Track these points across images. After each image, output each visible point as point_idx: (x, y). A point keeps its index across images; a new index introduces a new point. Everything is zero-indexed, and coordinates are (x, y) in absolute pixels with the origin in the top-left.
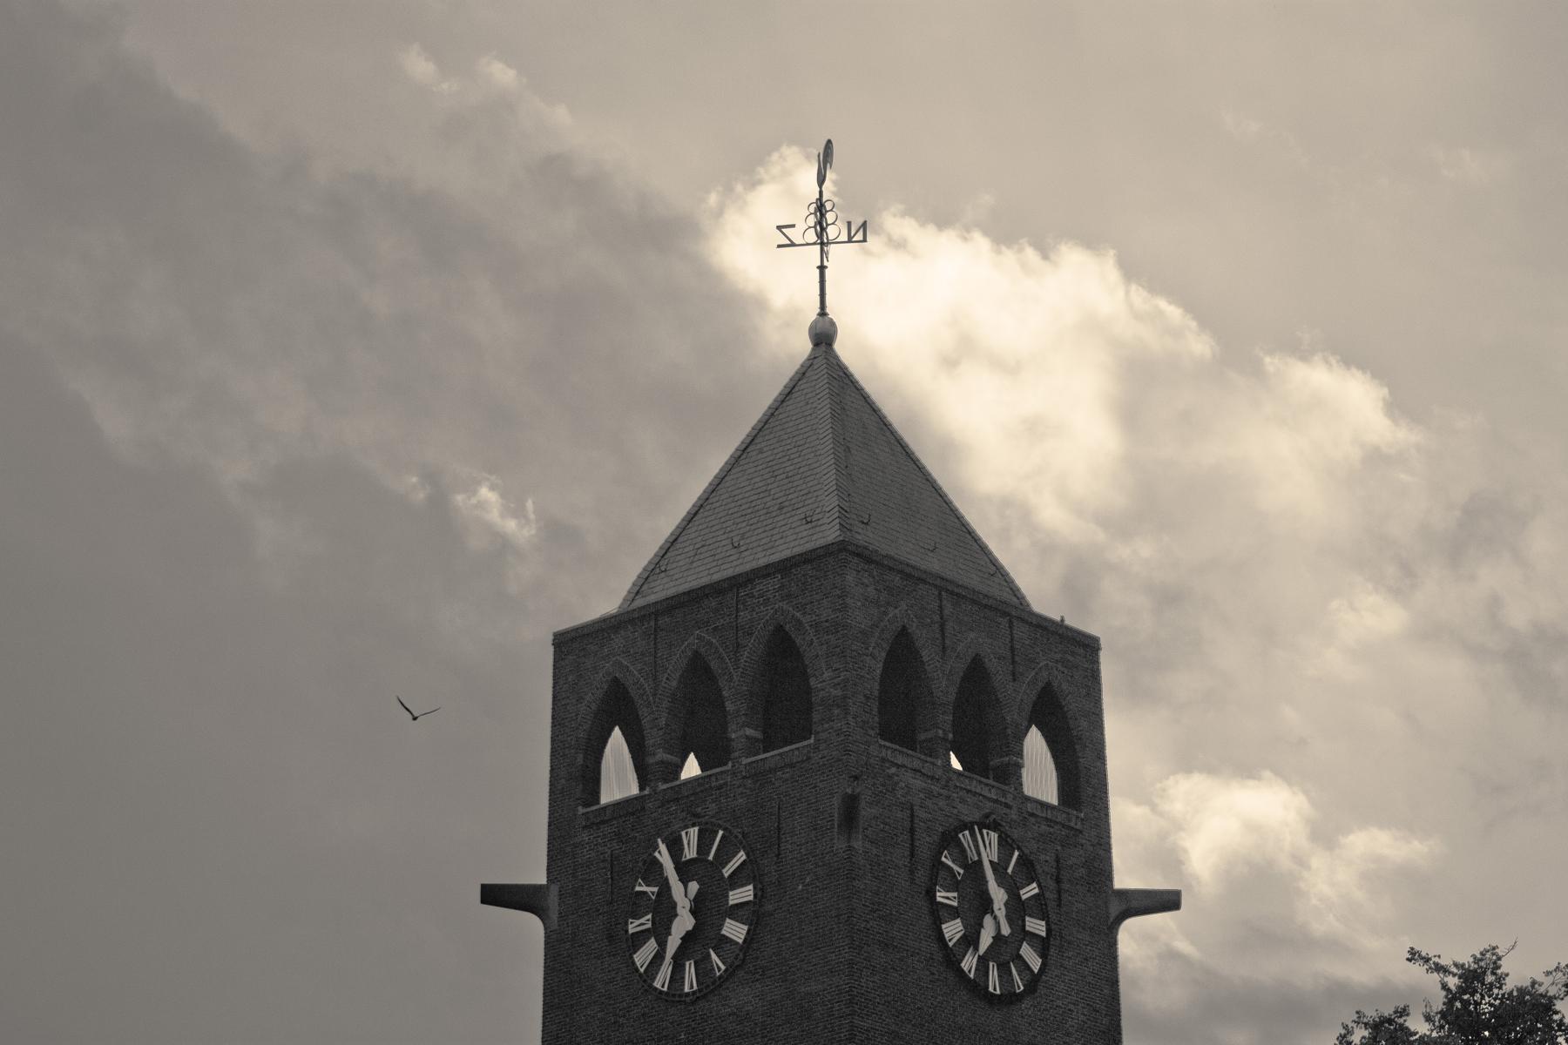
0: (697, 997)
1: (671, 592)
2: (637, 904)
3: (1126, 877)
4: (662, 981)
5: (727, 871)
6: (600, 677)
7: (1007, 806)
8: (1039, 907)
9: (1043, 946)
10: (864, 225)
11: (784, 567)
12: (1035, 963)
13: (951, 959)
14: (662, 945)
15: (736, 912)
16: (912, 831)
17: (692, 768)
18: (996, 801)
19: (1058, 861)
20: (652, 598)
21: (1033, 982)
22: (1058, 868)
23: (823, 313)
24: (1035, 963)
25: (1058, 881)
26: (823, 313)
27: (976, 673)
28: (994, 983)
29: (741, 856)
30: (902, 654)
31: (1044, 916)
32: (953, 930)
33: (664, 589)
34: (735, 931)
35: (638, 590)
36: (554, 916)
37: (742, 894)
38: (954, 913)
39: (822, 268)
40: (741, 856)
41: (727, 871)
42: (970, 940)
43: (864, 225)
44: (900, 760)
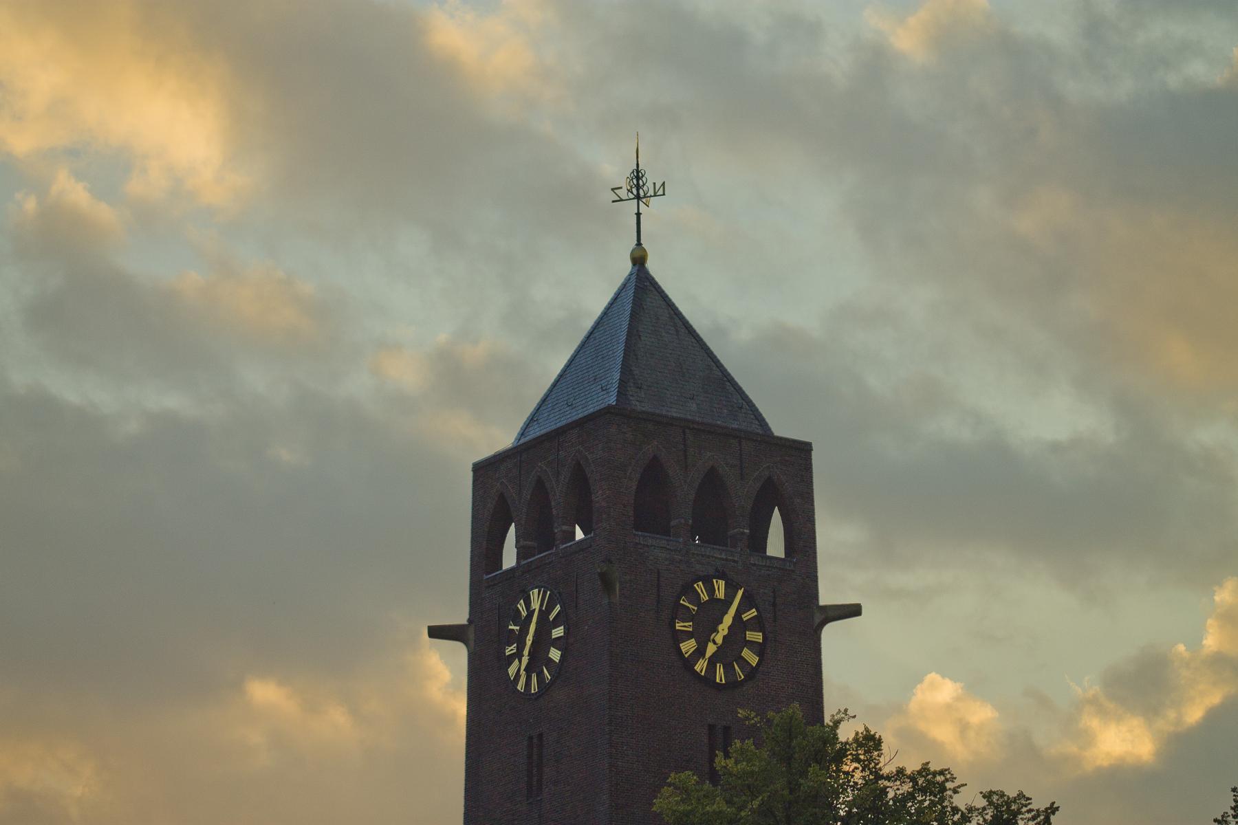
0: (538, 695)
1: (538, 434)
2: (510, 638)
3: (827, 596)
4: (520, 686)
5: (551, 617)
6: (500, 488)
7: (736, 562)
8: (757, 624)
9: (760, 649)
10: (664, 184)
11: (579, 424)
12: (754, 660)
13: (688, 664)
14: (520, 662)
15: (556, 643)
16: (658, 586)
17: (579, 535)
18: (726, 560)
19: (774, 592)
20: (528, 438)
21: (752, 673)
22: (775, 598)
23: (639, 244)
24: (754, 660)
25: (774, 605)
26: (639, 244)
27: (712, 479)
28: (720, 675)
29: (558, 608)
30: (653, 475)
31: (760, 628)
32: (688, 647)
33: (536, 432)
34: (555, 655)
35: (523, 433)
36: (472, 643)
37: (558, 632)
38: (689, 635)
39: (638, 214)
40: (558, 608)
41: (551, 617)
42: (700, 652)
43: (664, 184)
44: (650, 542)
